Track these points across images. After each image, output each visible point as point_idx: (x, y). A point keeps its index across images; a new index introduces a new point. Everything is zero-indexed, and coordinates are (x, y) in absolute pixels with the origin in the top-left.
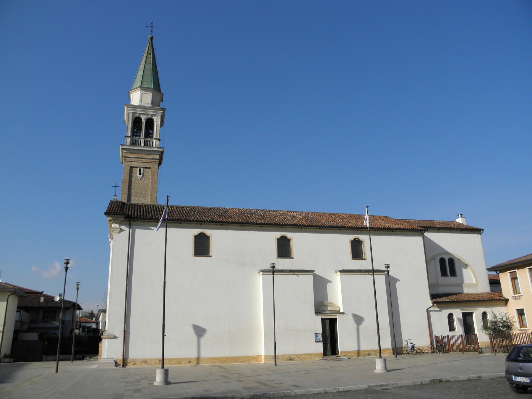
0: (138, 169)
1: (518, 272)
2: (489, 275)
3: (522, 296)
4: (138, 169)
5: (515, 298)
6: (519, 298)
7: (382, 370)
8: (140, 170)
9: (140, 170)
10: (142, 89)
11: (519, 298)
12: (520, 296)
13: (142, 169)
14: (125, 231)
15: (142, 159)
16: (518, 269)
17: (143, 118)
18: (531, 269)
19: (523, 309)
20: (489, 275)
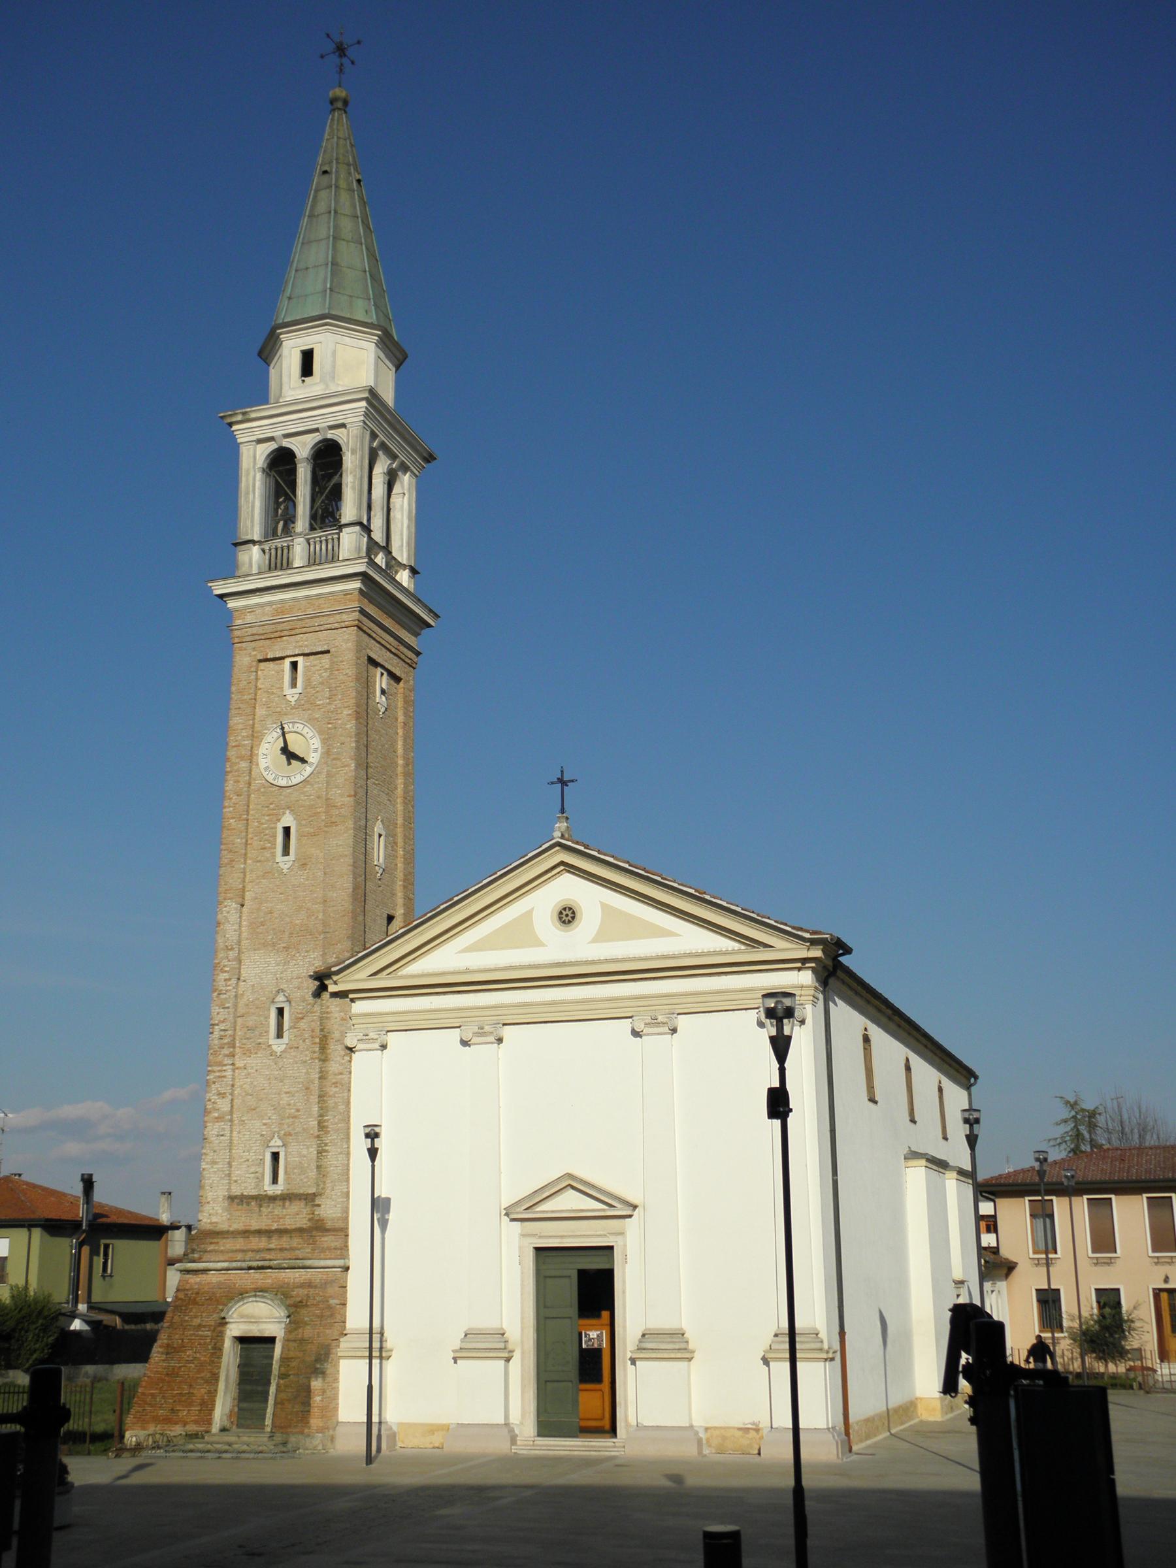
0: (287, 662)
1: (1117, 1203)
2: (541, 1252)
3: (1118, 1259)
4: (287, 662)
5: (1156, 1260)
6: (1109, 1262)
7: (799, 1490)
8: (294, 665)
9: (294, 665)
10: (385, 343)
11: (1109, 1264)
12: (1111, 1258)
13: (300, 660)
14: (589, 943)
15: (391, 639)
16: (1116, 1194)
17: (302, 448)
18: (1093, 1201)
19: (1118, 1290)
20: (541, 1252)
